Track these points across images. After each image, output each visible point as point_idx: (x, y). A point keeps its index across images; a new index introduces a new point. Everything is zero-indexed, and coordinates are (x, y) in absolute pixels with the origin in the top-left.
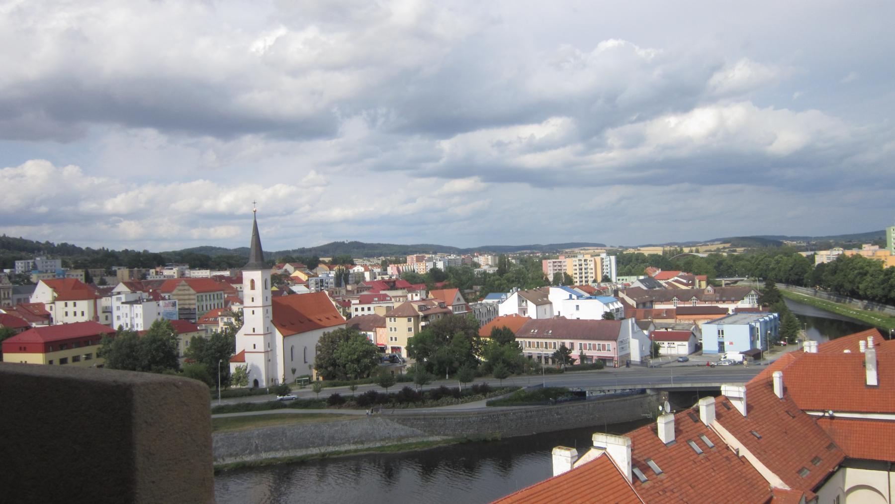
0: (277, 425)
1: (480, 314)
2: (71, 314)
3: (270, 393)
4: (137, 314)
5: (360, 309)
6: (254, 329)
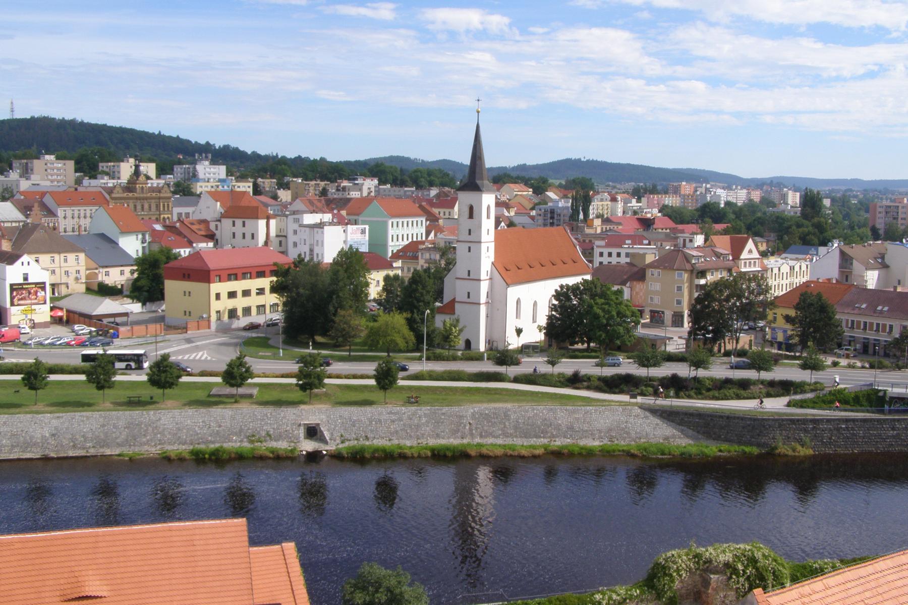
0: (541, 410)
1: (779, 274)
2: (239, 235)
3: (461, 359)
4: (317, 241)
6: (469, 272)
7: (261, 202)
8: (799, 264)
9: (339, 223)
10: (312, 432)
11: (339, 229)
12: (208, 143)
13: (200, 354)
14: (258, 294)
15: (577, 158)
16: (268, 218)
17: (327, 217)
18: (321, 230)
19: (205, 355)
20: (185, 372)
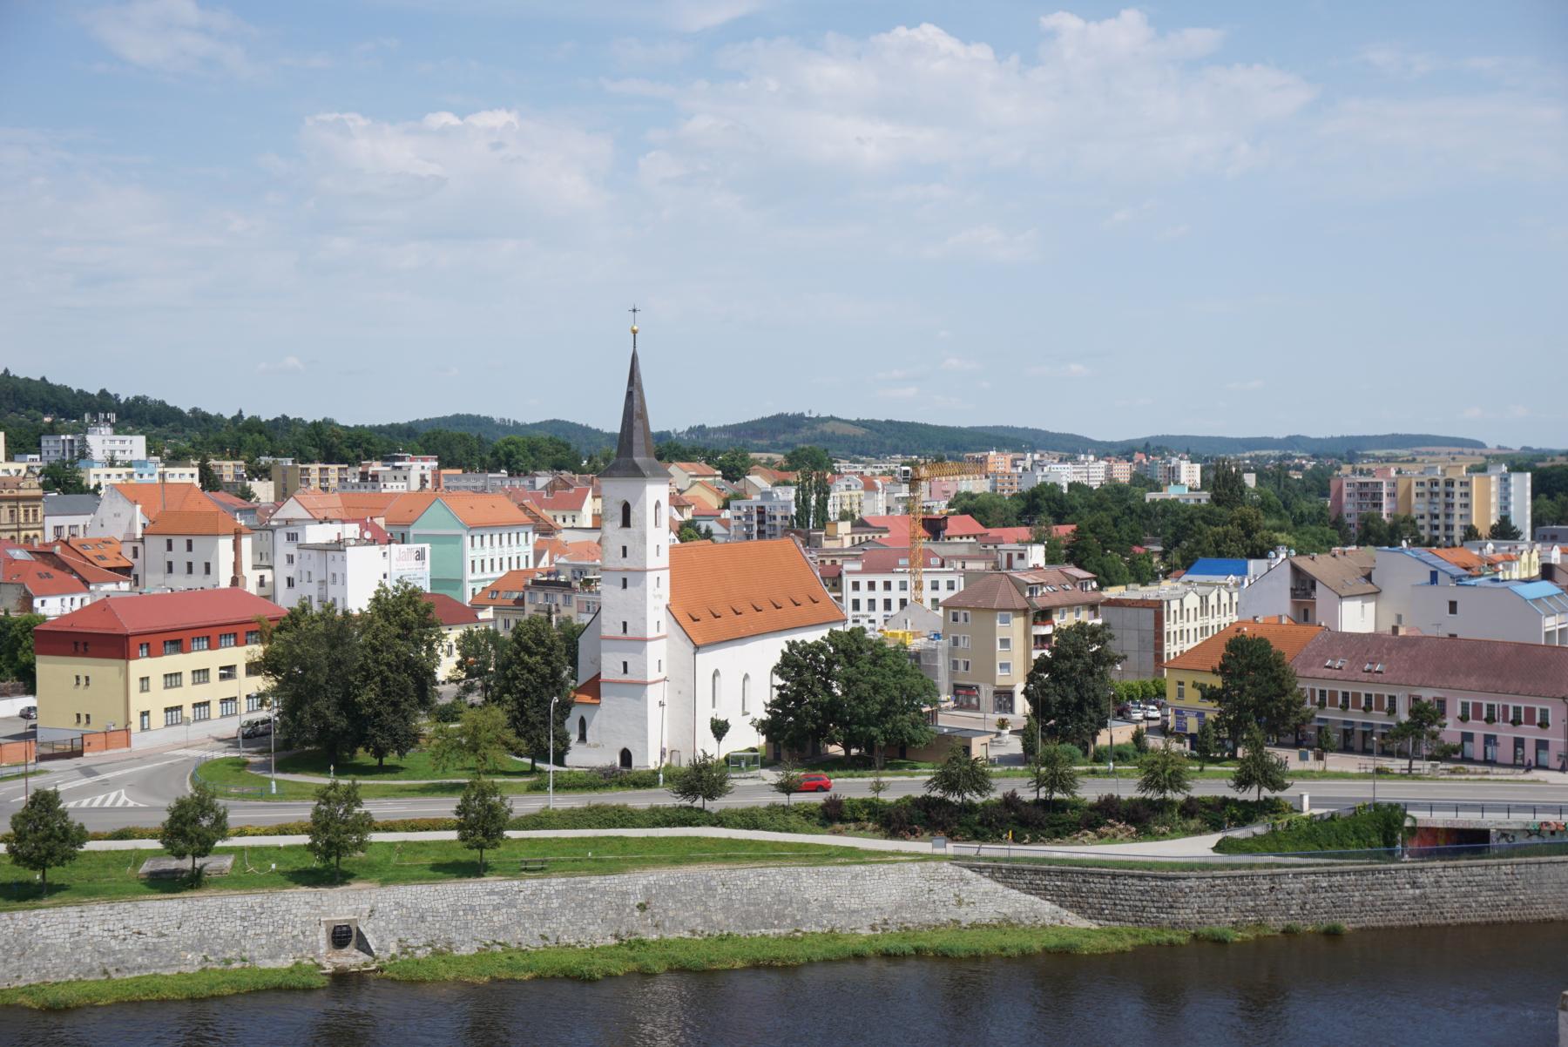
1: (1181, 610)
4: (334, 575)
5: (864, 585)
7: (220, 503)
8: (1216, 592)
9: (373, 542)
10: (341, 937)
11: (375, 550)
12: (103, 393)
13: (113, 795)
14: (222, 677)
15: (797, 412)
16: (237, 535)
17: (352, 530)
18: (342, 553)
19: (124, 798)
20: (82, 836)
